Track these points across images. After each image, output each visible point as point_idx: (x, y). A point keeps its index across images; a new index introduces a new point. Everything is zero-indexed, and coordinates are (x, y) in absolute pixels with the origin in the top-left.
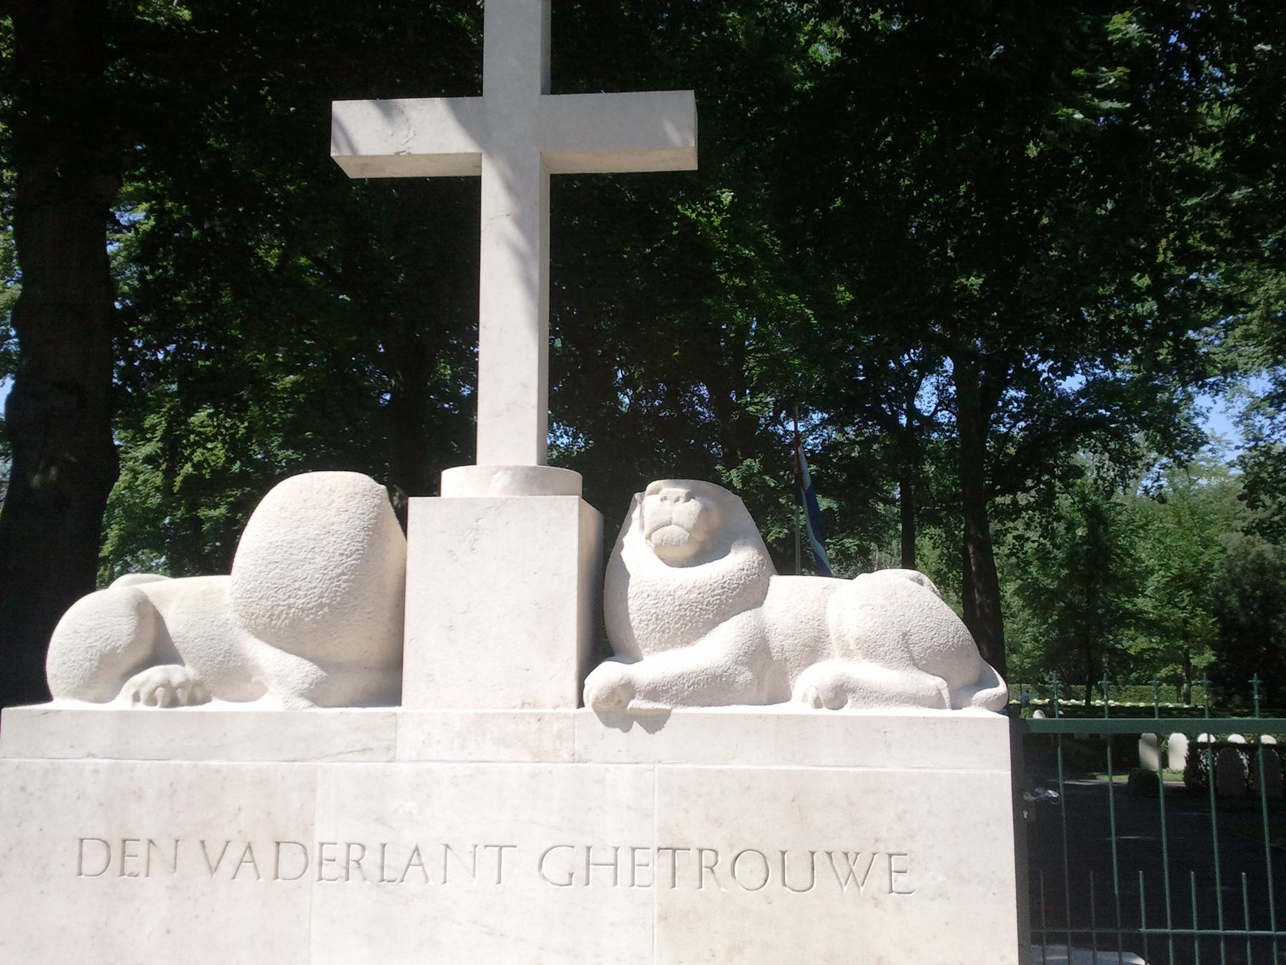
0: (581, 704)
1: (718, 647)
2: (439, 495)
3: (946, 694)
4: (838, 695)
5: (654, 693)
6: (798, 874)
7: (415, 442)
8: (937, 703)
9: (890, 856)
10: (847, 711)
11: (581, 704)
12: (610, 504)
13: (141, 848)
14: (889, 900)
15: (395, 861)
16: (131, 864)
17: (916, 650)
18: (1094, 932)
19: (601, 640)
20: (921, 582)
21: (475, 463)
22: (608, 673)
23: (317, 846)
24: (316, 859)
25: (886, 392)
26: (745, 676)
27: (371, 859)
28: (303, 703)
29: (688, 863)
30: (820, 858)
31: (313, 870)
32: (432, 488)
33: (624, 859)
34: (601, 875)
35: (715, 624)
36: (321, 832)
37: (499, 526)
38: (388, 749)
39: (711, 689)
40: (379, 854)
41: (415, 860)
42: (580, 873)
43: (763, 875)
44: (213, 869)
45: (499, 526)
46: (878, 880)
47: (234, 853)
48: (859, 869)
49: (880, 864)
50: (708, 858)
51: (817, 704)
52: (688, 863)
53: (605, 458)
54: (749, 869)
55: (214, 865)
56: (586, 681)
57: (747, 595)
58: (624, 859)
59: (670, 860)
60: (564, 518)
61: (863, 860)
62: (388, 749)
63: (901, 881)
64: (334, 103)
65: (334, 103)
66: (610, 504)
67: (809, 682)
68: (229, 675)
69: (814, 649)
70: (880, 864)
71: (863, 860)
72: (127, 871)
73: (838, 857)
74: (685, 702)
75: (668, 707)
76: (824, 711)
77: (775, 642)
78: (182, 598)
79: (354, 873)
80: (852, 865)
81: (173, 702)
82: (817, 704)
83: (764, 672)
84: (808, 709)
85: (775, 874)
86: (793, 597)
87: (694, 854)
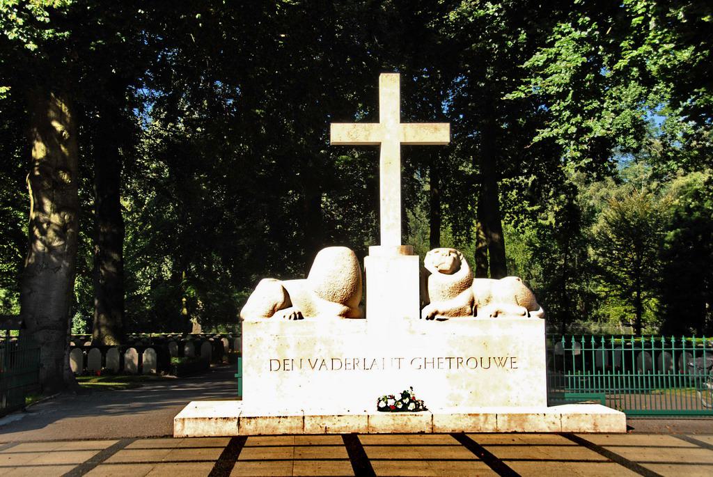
0: (421, 318)
1: (462, 300)
6: (486, 364)
7: (361, 237)
11: (421, 318)
13: (290, 362)
14: (510, 370)
16: (287, 367)
17: (519, 301)
18: (673, 348)
19: (424, 301)
22: (428, 311)
29: (454, 362)
30: (492, 360)
33: (436, 361)
34: (429, 366)
37: (390, 263)
44: (313, 368)
46: (508, 365)
47: (319, 363)
48: (503, 362)
49: (509, 360)
50: (460, 360)
52: (454, 362)
53: (412, 241)
54: (472, 363)
55: (313, 366)
58: (436, 361)
61: (504, 360)
63: (514, 365)
64: (332, 124)
65: (332, 124)
70: (509, 360)
71: (504, 360)
73: (497, 359)
80: (501, 362)
86: (482, 286)
87: (456, 359)
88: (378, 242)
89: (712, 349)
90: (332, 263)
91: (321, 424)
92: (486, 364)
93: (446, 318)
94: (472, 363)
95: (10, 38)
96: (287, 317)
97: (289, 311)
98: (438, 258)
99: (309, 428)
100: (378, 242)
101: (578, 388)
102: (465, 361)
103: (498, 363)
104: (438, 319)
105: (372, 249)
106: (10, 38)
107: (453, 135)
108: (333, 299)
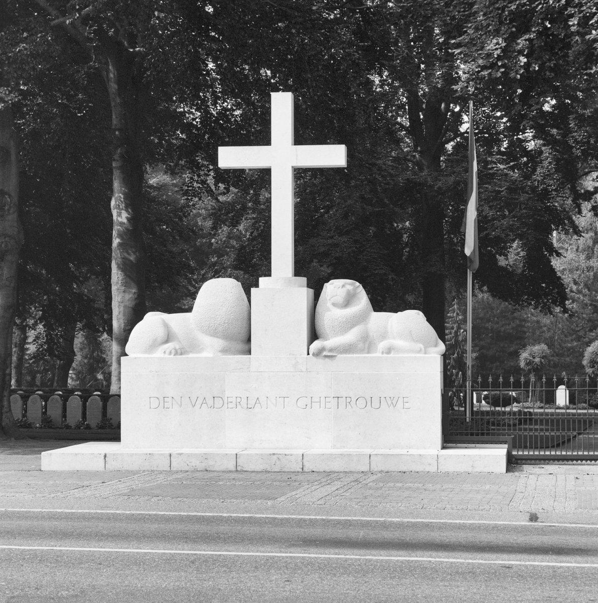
0: (308, 354)
1: (351, 336)
2: (258, 287)
3: (423, 349)
4: (389, 350)
5: (331, 350)
6: (376, 403)
7: (251, 266)
8: (420, 351)
9: (404, 398)
10: (391, 355)
11: (308, 354)
12: (316, 287)
13: (170, 400)
15: (252, 402)
19: (314, 335)
20: (419, 314)
21: (270, 275)
22: (316, 344)
23: (226, 399)
24: (226, 402)
25: (449, 209)
26: (361, 345)
27: (244, 401)
28: (220, 354)
30: (383, 399)
31: (226, 405)
32: (257, 286)
33: (323, 399)
35: (351, 328)
36: (227, 394)
37: (281, 288)
38: (248, 368)
39: (348, 349)
40: (246, 400)
41: (204, 402)
42: (309, 406)
43: (365, 405)
44: (194, 406)
45: (281, 288)
47: (200, 401)
48: (394, 402)
49: (401, 400)
50: (349, 400)
51: (383, 353)
53: (314, 268)
54: (361, 403)
56: (310, 347)
57: (361, 319)
58: (323, 399)
59: (283, 400)
60: (301, 292)
62: (248, 368)
63: (407, 405)
66: (316, 287)
67: (382, 345)
68: (192, 347)
69: (384, 336)
72: (165, 407)
73: (388, 399)
74: (341, 353)
75: (336, 355)
76: (385, 355)
77: (371, 334)
78: (175, 320)
79: (239, 406)
81: (176, 354)
82: (383, 353)
83: (366, 344)
84: (380, 355)
85: (369, 403)
88: (268, 274)
89: (0, 473)
90: (217, 294)
91: (188, 462)
92: (376, 403)
93: (334, 354)
94: (361, 403)
95: (500, 263)
96: (167, 352)
97: (170, 346)
98: (335, 289)
99: (175, 466)
100: (268, 274)
101: (500, 429)
102: (354, 400)
103: (389, 403)
104: (326, 356)
105: (262, 280)
106: (500, 263)
107: (280, 90)
108: (214, 334)
